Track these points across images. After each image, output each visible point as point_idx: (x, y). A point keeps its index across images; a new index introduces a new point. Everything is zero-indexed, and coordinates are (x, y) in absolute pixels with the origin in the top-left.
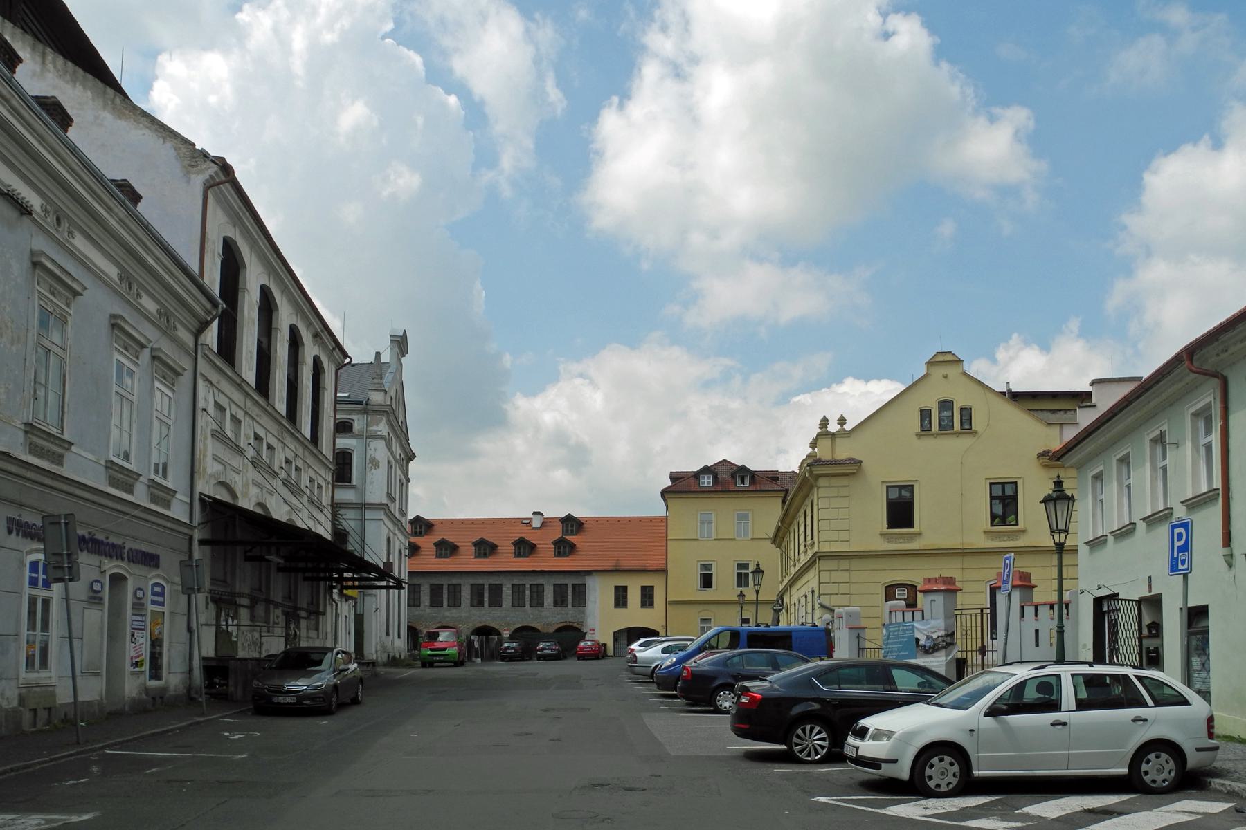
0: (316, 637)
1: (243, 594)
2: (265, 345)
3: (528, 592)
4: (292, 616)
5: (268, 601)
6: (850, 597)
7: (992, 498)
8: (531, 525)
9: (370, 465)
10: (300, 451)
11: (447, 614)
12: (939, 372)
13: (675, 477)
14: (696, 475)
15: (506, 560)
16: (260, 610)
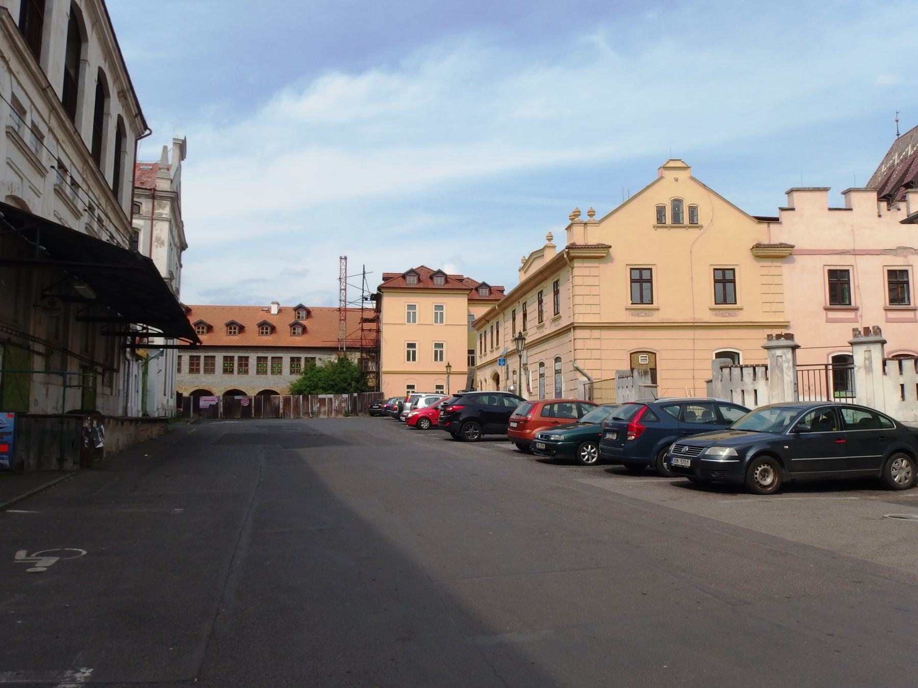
0: (110, 394)
1: (39, 339)
2: (72, 72)
3: (269, 363)
4: (88, 367)
5: (65, 352)
6: (601, 362)
7: (716, 281)
8: (270, 312)
9: (156, 243)
10: (103, 202)
11: (203, 379)
12: (670, 175)
13: (386, 278)
14: (404, 276)
15: (253, 337)
16: (56, 361)
